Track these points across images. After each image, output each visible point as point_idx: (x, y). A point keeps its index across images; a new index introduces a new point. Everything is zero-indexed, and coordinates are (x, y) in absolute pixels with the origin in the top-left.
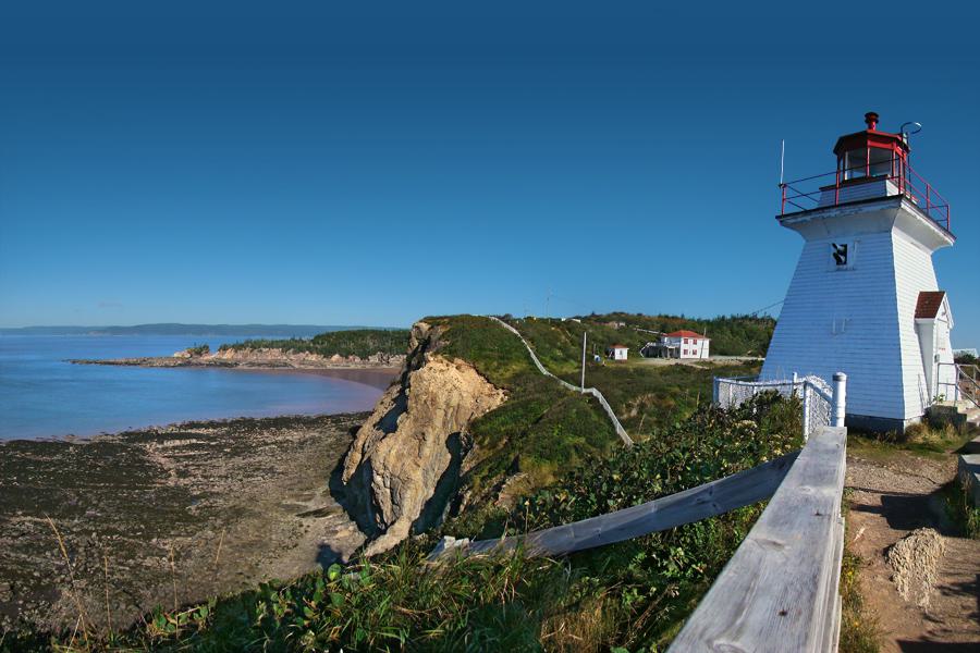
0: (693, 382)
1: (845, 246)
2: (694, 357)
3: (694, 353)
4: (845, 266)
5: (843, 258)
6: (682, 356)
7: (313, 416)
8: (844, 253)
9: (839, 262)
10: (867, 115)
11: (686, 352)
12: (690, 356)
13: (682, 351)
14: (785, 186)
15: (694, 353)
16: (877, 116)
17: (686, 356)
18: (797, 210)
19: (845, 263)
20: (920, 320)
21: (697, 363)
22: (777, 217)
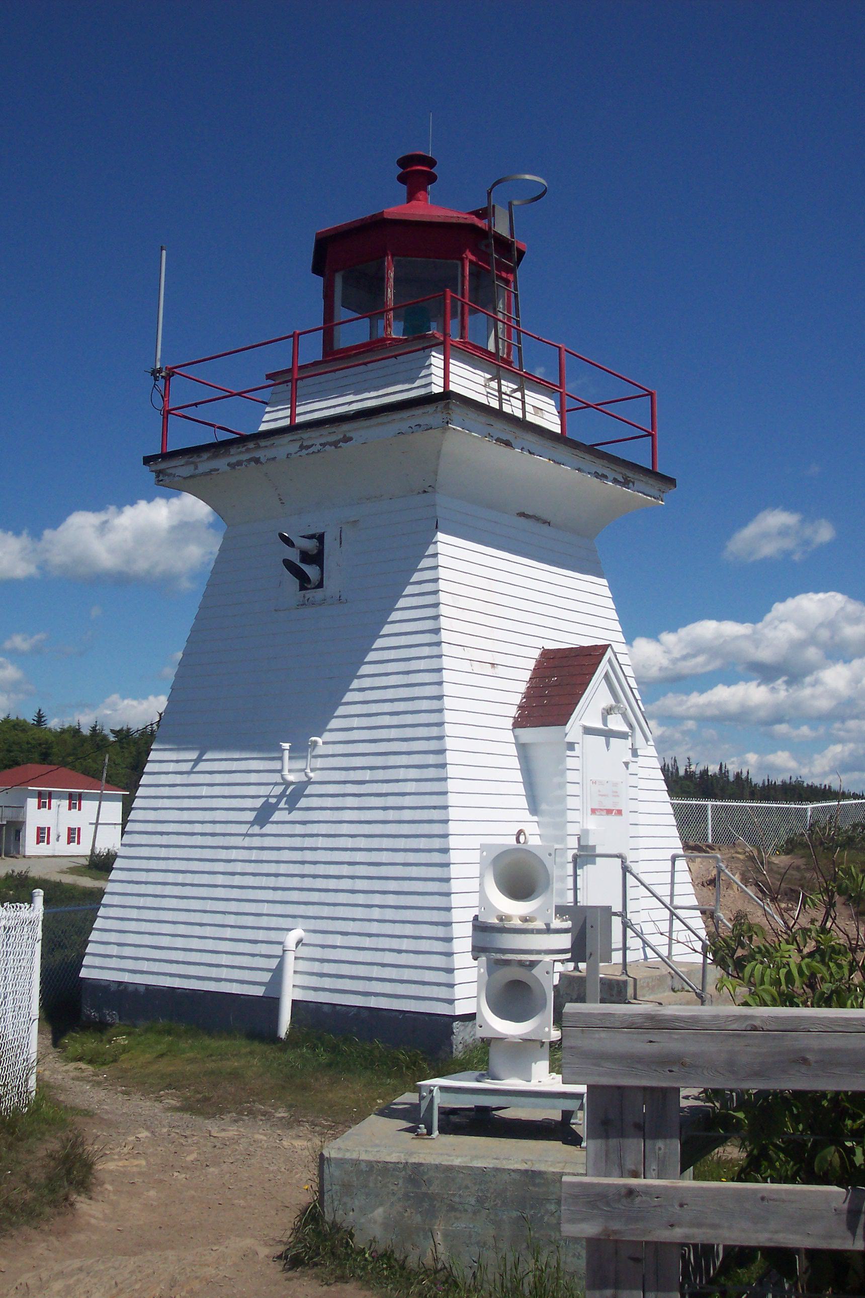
0: (250, 1195)
1: (320, 538)
2: (73, 849)
3: (73, 835)
4: (318, 594)
5: (311, 571)
6: (31, 847)
7: (531, 514)
8: (316, 558)
9: (304, 581)
10: (405, 162)
11: (42, 835)
12: (60, 847)
13: (30, 834)
14: (171, 373)
15: (73, 835)
16: (431, 163)
17: (44, 849)
18: (207, 437)
19: (320, 585)
20: (530, 734)
21: (76, 871)
22: (147, 460)
